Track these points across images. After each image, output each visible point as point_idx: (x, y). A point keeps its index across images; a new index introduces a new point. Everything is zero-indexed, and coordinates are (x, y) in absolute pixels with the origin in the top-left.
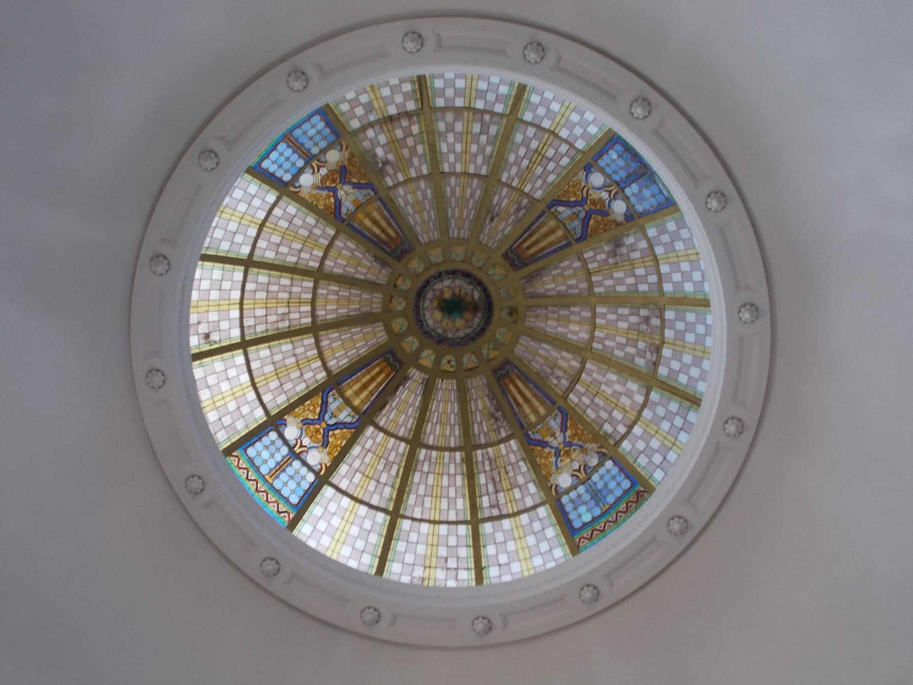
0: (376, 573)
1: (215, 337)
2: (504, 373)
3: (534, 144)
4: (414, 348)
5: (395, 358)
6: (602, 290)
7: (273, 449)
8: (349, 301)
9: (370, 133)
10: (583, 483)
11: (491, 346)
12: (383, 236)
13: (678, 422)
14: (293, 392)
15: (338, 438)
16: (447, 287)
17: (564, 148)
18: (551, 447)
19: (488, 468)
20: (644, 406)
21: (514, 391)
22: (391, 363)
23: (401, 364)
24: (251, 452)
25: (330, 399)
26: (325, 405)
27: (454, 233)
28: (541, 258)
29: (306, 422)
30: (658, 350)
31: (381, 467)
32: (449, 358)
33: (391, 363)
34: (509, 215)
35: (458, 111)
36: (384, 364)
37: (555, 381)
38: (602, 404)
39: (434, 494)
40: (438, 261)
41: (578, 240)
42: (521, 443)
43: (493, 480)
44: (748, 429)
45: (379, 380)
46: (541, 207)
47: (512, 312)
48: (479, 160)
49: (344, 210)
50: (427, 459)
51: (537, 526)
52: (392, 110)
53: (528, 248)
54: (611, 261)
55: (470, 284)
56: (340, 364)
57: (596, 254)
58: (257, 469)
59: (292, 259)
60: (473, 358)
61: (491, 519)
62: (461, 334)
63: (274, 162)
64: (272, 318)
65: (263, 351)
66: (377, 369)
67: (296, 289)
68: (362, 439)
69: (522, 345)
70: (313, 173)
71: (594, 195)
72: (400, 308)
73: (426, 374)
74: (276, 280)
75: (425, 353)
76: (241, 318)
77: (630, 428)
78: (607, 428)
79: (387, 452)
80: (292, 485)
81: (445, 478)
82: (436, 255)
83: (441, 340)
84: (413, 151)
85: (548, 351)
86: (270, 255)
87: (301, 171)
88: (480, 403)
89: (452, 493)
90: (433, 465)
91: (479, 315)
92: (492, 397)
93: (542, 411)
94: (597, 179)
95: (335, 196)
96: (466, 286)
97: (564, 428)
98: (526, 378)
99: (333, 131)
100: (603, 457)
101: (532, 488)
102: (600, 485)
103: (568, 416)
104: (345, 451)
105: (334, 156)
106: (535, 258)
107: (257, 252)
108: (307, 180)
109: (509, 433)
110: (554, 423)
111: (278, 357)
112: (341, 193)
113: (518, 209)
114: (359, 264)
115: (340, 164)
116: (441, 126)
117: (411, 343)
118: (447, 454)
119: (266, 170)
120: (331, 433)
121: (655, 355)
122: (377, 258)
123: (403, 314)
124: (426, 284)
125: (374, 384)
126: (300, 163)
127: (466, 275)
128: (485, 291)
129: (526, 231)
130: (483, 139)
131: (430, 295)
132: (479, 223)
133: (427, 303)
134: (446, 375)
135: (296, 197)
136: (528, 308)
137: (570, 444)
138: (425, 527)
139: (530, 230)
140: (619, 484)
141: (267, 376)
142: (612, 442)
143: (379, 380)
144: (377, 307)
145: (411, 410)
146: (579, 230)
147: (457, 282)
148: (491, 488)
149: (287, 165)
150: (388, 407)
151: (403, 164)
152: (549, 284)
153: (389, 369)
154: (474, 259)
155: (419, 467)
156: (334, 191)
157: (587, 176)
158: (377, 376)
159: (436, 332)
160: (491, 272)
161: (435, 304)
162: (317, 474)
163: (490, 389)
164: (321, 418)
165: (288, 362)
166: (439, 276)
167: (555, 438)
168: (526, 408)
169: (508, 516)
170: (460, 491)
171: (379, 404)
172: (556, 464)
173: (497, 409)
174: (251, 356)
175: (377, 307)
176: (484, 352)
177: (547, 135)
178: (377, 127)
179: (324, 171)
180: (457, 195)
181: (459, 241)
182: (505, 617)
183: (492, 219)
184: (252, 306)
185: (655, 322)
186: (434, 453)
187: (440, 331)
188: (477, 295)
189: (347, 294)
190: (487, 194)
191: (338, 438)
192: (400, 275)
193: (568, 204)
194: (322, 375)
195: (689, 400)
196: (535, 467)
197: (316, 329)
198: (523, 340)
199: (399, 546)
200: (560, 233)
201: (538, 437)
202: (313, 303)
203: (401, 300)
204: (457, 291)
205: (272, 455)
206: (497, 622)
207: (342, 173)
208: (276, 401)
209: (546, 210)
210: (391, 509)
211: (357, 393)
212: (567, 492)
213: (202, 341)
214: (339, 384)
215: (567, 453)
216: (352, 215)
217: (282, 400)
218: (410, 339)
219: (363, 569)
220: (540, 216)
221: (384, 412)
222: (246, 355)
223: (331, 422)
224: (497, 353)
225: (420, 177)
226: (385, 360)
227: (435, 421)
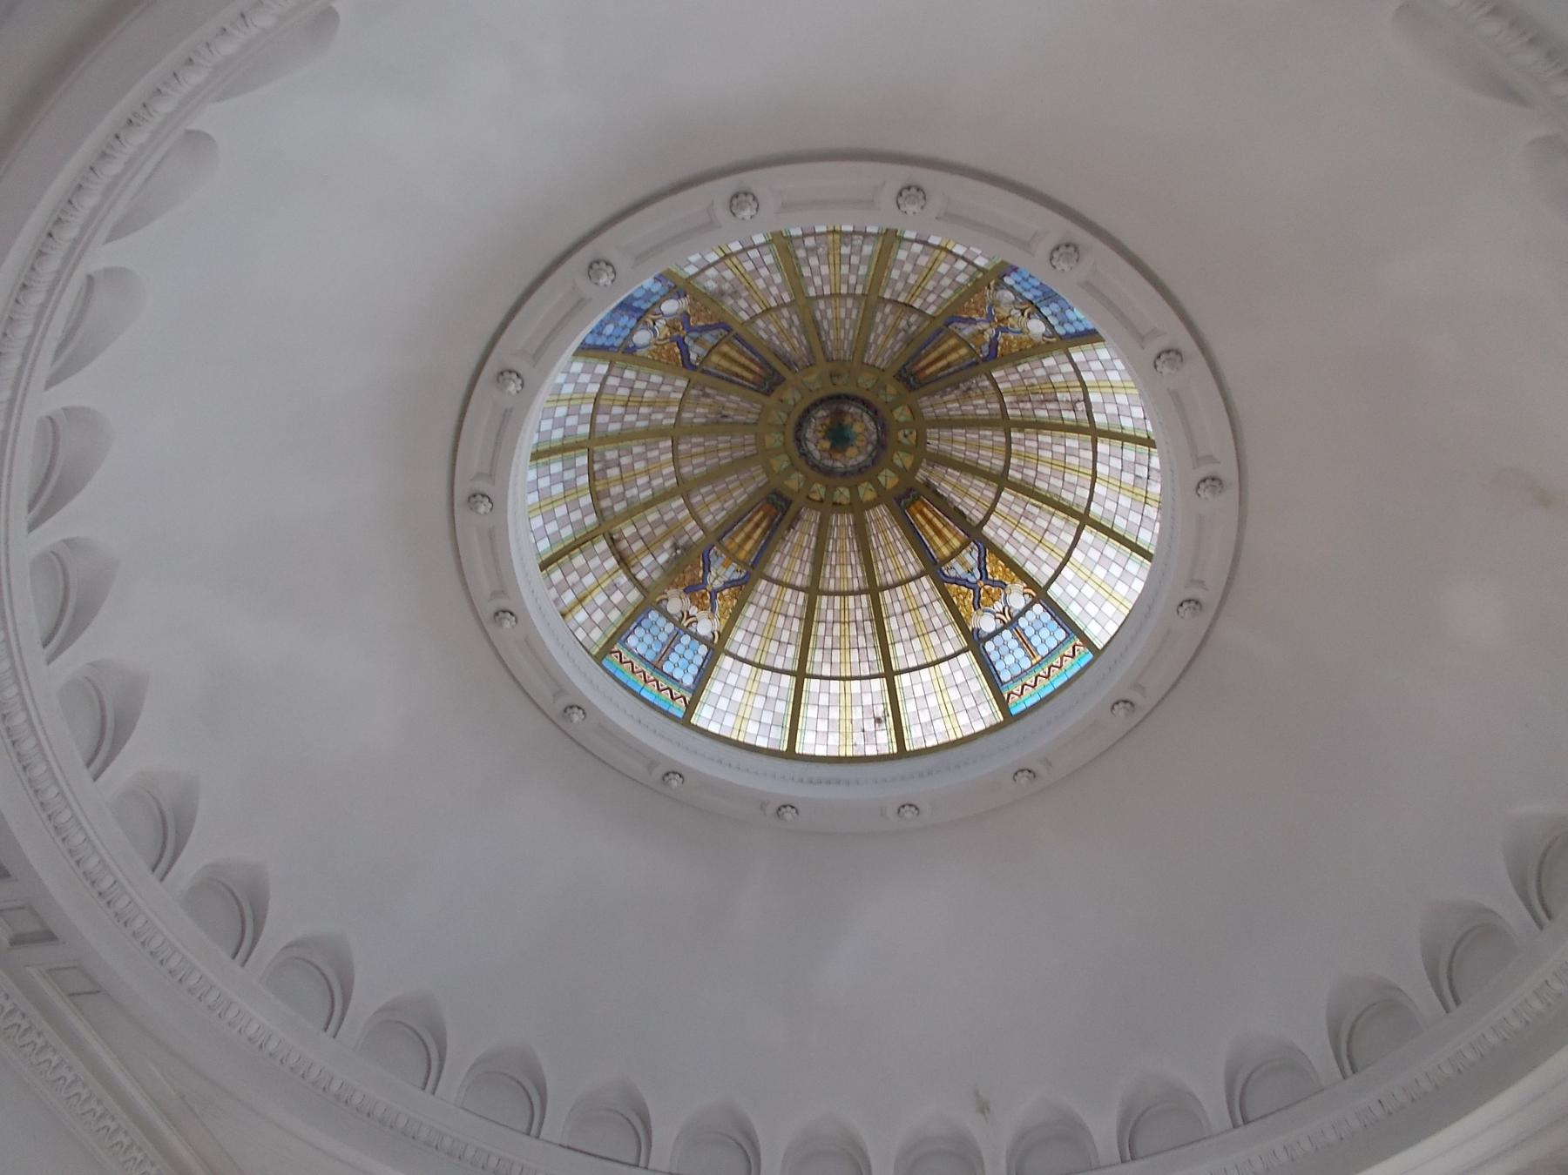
1: (879, 712)
2: (911, 379)
3: (617, 410)
7: (1004, 650)
8: (842, 551)
9: (642, 576)
14: (943, 617)
15: (996, 569)
16: (817, 445)
17: (613, 381)
19: (1029, 405)
21: (933, 369)
23: (911, 490)
24: (1005, 676)
25: (953, 573)
26: (958, 581)
27: (750, 450)
28: (761, 358)
29: (977, 604)
32: (901, 435)
33: (910, 501)
35: (596, 497)
41: (729, 330)
42: (996, 367)
43: (1043, 402)
48: (653, 454)
49: (736, 576)
52: (611, 562)
53: (752, 371)
54: (745, 294)
55: (809, 422)
57: (742, 309)
58: (1024, 672)
59: (796, 625)
60: (899, 410)
62: (871, 426)
63: (686, 671)
64: (862, 642)
65: (897, 651)
67: (830, 617)
68: (998, 542)
72: (847, 493)
75: (898, 462)
76: (860, 678)
77: (957, 257)
80: (1044, 633)
82: (780, 463)
83: (881, 445)
84: (654, 525)
86: (792, 651)
87: (695, 636)
88: (952, 406)
91: (846, 408)
93: (952, 342)
94: (642, 337)
95: (720, 590)
97: (971, 321)
98: (916, 357)
104: (1011, 564)
105: (675, 605)
106: (765, 364)
107: (788, 667)
108: (705, 627)
111: (905, 634)
112: (717, 584)
113: (707, 396)
117: (888, 479)
122: (791, 526)
123: (854, 489)
125: (935, 520)
128: (815, 405)
129: (732, 381)
130: (625, 460)
131: (829, 463)
133: (838, 464)
134: (921, 439)
135: (724, 635)
139: (729, 379)
142: (980, 275)
144: (847, 519)
146: (716, 332)
148: (1052, 406)
151: (674, 528)
152: (794, 346)
156: (714, 593)
158: (926, 517)
160: (791, 402)
161: (838, 456)
165: (909, 622)
166: (805, 455)
171: (958, 517)
174: (903, 666)
175: (847, 519)
178: (633, 571)
179: (693, 610)
182: (1198, 460)
185: (810, 242)
186: (1013, 461)
187: (870, 448)
188: (822, 413)
190: (693, 430)
191: (996, 569)
193: (685, 352)
194: (925, 582)
197: (873, 590)
199: (1120, 525)
200: (725, 348)
201: (985, 348)
205: (1010, 651)
207: (693, 589)
208: (952, 639)
211: (946, 542)
217: (952, 631)
218: (882, 479)
219: (1144, 576)
220: (709, 373)
223: (978, 575)
225: (688, 505)
226: (908, 508)
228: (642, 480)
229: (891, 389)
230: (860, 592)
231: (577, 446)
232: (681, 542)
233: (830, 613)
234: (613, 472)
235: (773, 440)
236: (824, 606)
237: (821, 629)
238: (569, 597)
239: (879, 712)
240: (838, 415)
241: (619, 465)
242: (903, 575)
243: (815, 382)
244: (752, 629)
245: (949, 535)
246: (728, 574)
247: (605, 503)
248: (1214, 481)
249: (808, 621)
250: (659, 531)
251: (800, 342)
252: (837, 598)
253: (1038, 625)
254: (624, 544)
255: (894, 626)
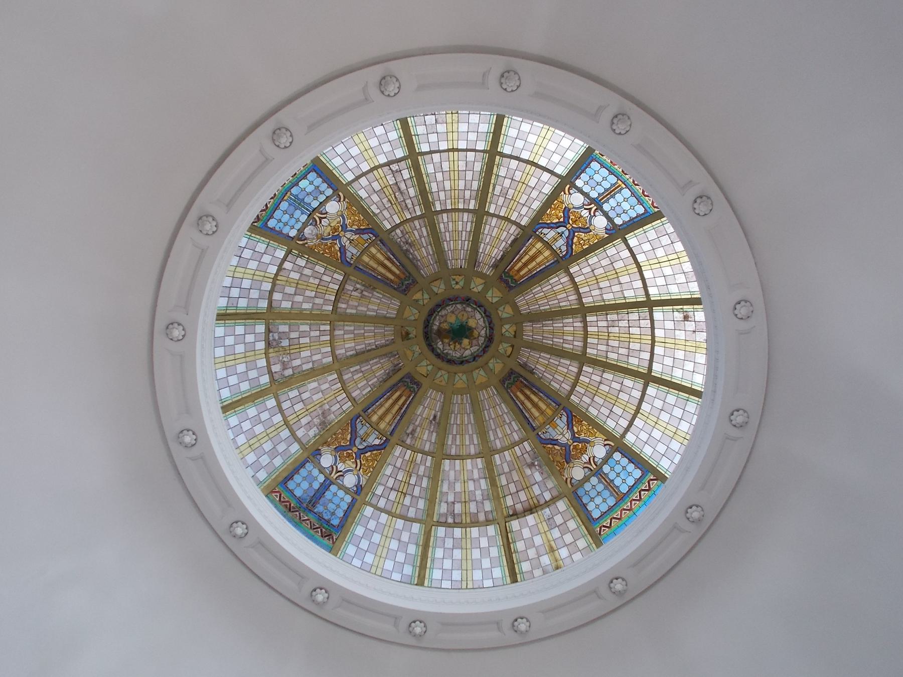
0: (504, 117)
1: (679, 316)
2: (405, 283)
3: (407, 501)
4: (490, 292)
5: (506, 282)
6: (330, 378)
9: (548, 496)
10: (314, 209)
11: (421, 303)
12: (528, 393)
13: (235, 292)
15: (554, 216)
16: (467, 348)
18: (351, 231)
20: (271, 292)
22: (509, 277)
24: (640, 210)
25: (564, 248)
26: (569, 244)
27: (466, 398)
29: (587, 230)
30: (269, 345)
31: (511, 192)
32: (458, 287)
34: (420, 425)
35: (475, 523)
36: (516, 278)
37: (358, 286)
38: (311, 280)
39: (456, 173)
40: (477, 371)
41: (358, 416)
44: (162, 332)
45: (520, 264)
46: (393, 440)
47: (406, 336)
49: (564, 419)
50: (467, 201)
51: (351, 164)
52: (530, 519)
56: (557, 279)
57: (340, 408)
58: (633, 194)
59: (608, 376)
60: (435, 289)
61: (398, 161)
62: (449, 309)
64: (624, 324)
65: (630, 295)
66: (522, 273)
67: (603, 348)
68: (532, 214)
69: (394, 309)
70: (594, 457)
71: (350, 464)
73: (477, 271)
74: (621, 358)
78: (301, 262)
79: (506, 204)
80: (598, 178)
81: (448, 187)
82: (480, 376)
83: (467, 301)
85: (368, 310)
86: (628, 382)
87: (605, 460)
88: (424, 253)
89: (439, 176)
90: (461, 196)
91: (435, 328)
92: (413, 261)
94: (350, 481)
95: (573, 433)
96: (450, 352)
97: (343, 249)
99: (579, 498)
100: (300, 236)
101: (363, 194)
102: (297, 213)
103: (341, 261)
105: (578, 473)
108: (599, 451)
109: (393, 234)
110: (352, 251)
111: (616, 288)
112: (568, 435)
113: (414, 431)
114: (546, 366)
115: (571, 465)
116: (488, 506)
117: (493, 296)
118: (449, 207)
119: (637, 467)
120: (562, 220)
121: (271, 338)
122: (532, 372)
123: (503, 321)
124: (485, 350)
125: (523, 260)
126: (606, 469)
127: (450, 361)
128: (433, 350)
130: (451, 498)
132: (446, 410)
133: (483, 332)
134: (459, 272)
135: (609, 436)
136: (393, 342)
137: (335, 238)
138: (462, 145)
139: (402, 415)
140: (280, 221)
141: (626, 273)
143: (520, 264)
144: (528, 327)
145: (488, 240)
146: (359, 426)
147: (458, 355)
148: (403, 186)
149: (618, 468)
150: (509, 242)
151: (518, 465)
152: (379, 369)
153: (511, 273)
154: (446, 377)
155: (474, 193)
156: (574, 438)
157: (359, 481)
158: (522, 268)
159: (472, 308)
161: (476, 333)
162: (573, 186)
163: (416, 267)
164: (572, 232)
165: (607, 284)
166: (475, 358)
167: (349, 239)
168: (381, 258)
169: (381, 166)
170: (432, 179)
171: (518, 244)
172: (344, 218)
173: (407, 250)
175: (528, 327)
176: (426, 296)
177: (398, 512)
180: (467, 437)
181: (460, 392)
182: (367, 100)
183: (435, 417)
184: (643, 337)
186: (461, 206)
187: (469, 309)
189: (555, 340)
191: (554, 216)
192: (509, 357)
193: (372, 448)
194: (574, 269)
195: (229, 315)
196: (364, 211)
198: (393, 313)
200: (375, 418)
201: (365, 237)
202: (586, 334)
203: (507, 334)
204: (458, 346)
206: (374, 92)
207: (568, 457)
208: (616, 250)
209: (389, 437)
210: (498, 158)
211: (540, 252)
212: (328, 199)
213: (691, 314)
214: (557, 262)
215: (335, 229)
216: (555, 413)
218: (495, 300)
221: (513, 237)
222: (647, 294)
223: (562, 229)
224: (414, 298)
227: (464, 233)
228: (471, 486)
229: (418, 296)
230: (584, 321)
231: (428, 535)
232: (529, 460)
233: (600, 347)
234: (458, 508)
235: (461, 380)
236: (595, 352)
237: (612, 356)
238: (546, 560)
239: (679, 316)
240: (440, 333)
241: (453, 503)
242: (569, 286)
243: (418, 348)
244: (607, 412)
245: (534, 251)
246: (562, 425)
247: (482, 517)
248: (382, 83)
249: (605, 366)
250: (516, 478)
251: (376, 363)
252: (589, 340)
253: (592, 182)
254: (519, 507)
255: (611, 296)
